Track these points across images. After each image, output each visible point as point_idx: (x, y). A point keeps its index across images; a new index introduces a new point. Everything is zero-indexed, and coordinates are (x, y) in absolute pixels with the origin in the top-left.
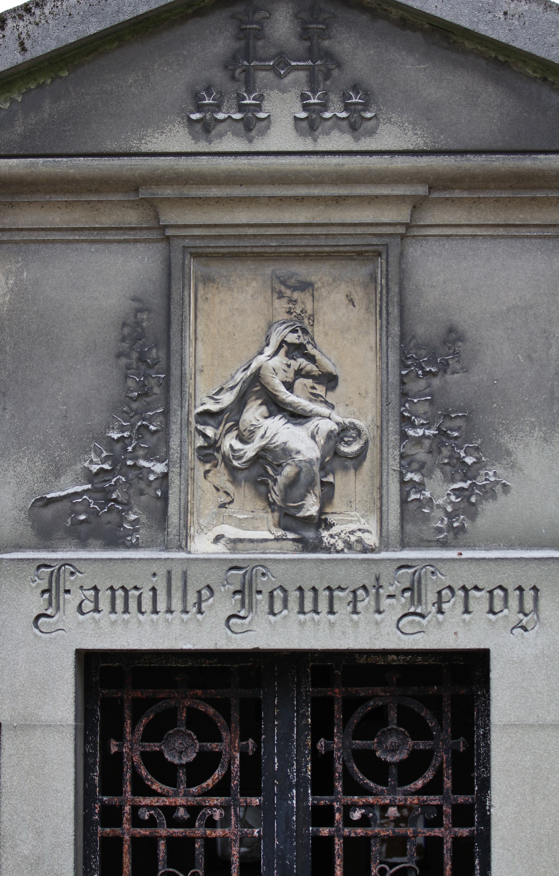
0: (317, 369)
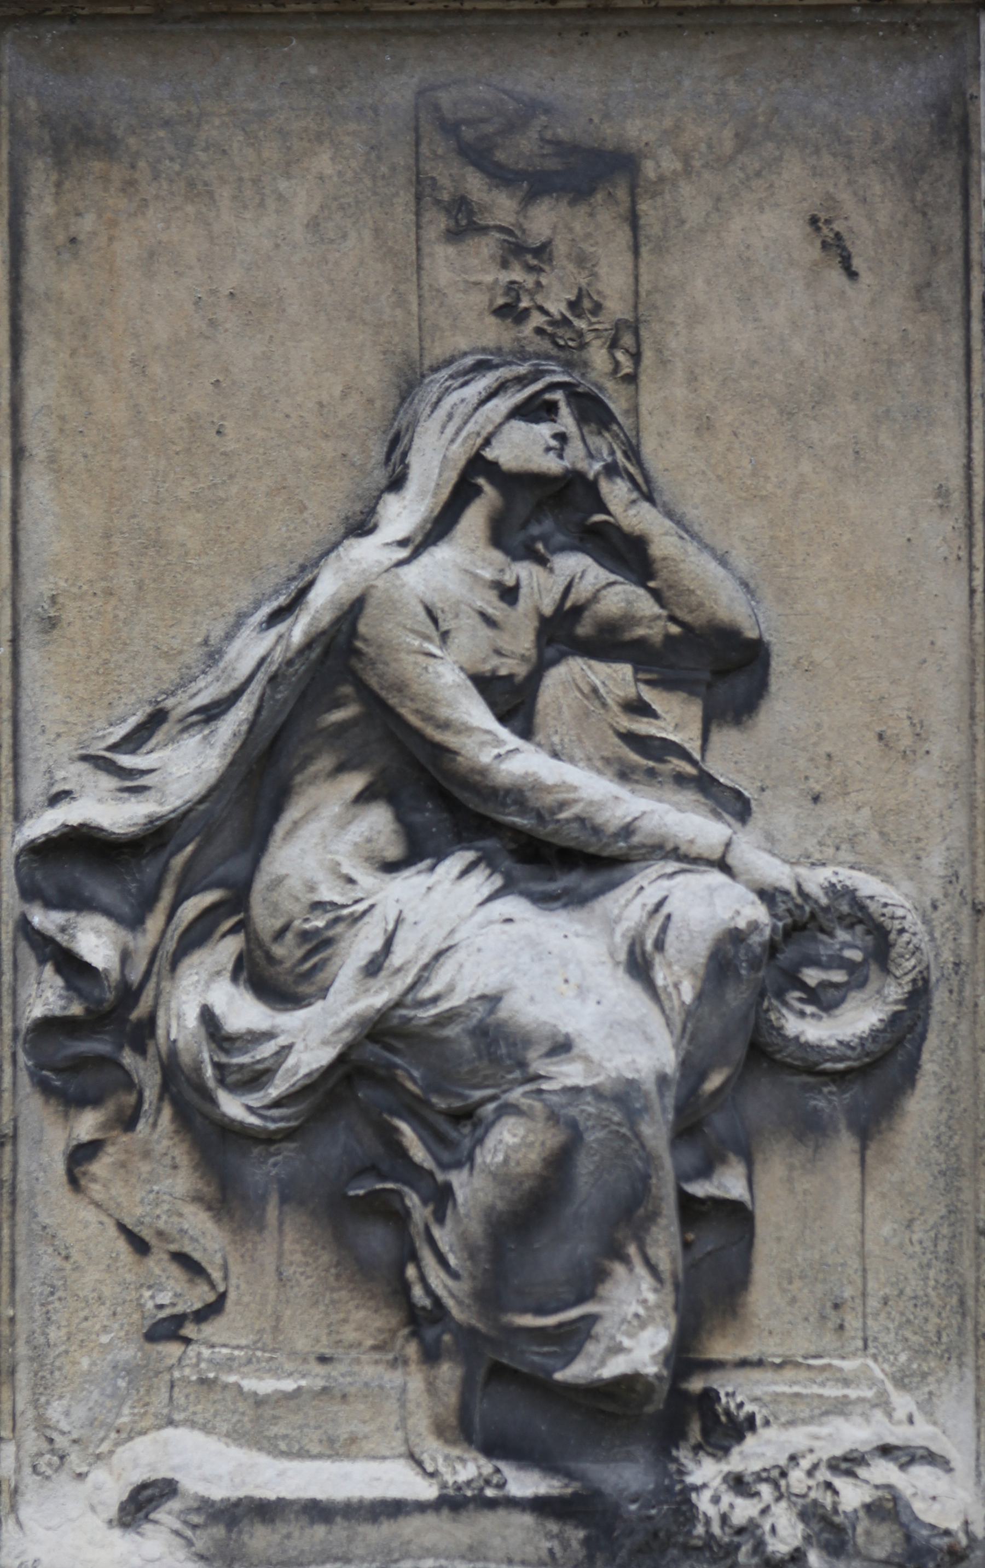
0: (657, 610)
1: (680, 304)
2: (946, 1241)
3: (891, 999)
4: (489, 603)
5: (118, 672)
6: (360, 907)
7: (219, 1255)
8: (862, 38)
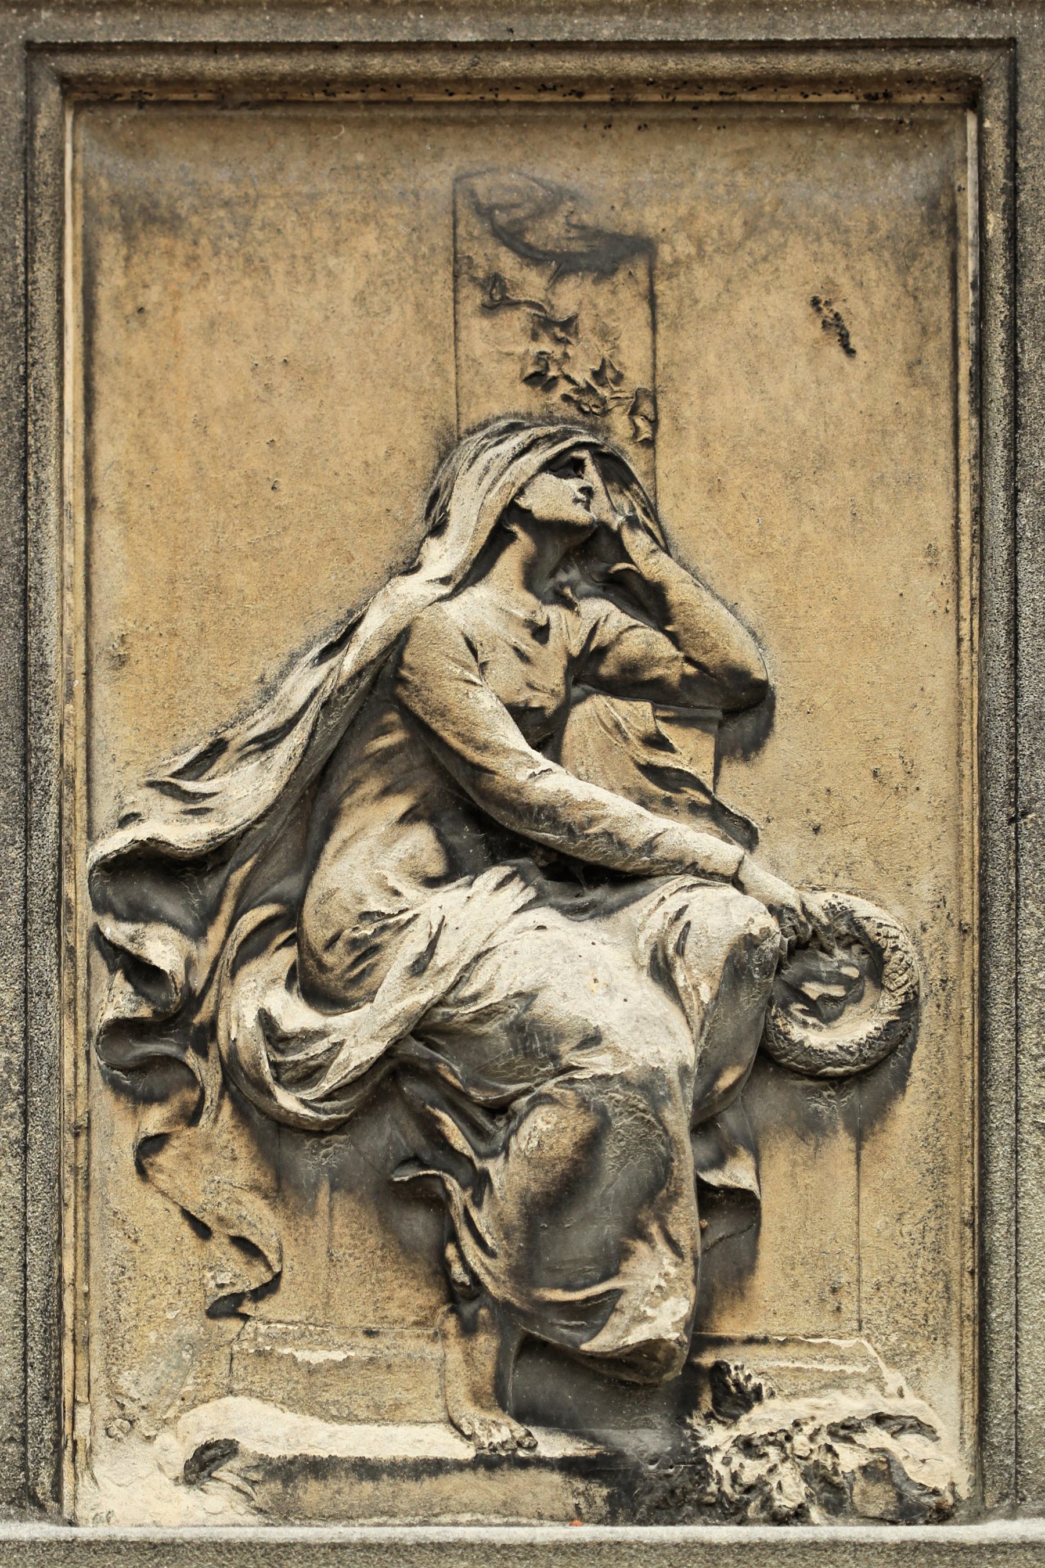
0: (674, 652)
1: (693, 375)
2: (933, 1233)
3: (886, 1010)
4: (522, 640)
5: (182, 706)
6: (405, 917)
7: (275, 1239)
8: (859, 136)
